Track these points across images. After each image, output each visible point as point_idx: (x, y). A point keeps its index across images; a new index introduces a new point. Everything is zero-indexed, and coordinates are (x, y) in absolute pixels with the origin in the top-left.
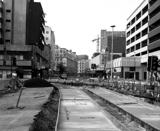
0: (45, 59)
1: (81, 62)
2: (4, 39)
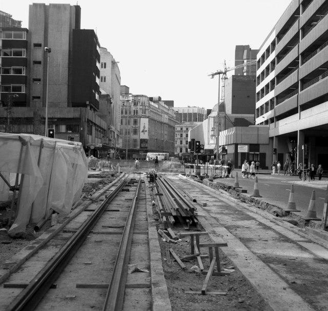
0: (100, 128)
1: (182, 129)
2: (30, 94)
